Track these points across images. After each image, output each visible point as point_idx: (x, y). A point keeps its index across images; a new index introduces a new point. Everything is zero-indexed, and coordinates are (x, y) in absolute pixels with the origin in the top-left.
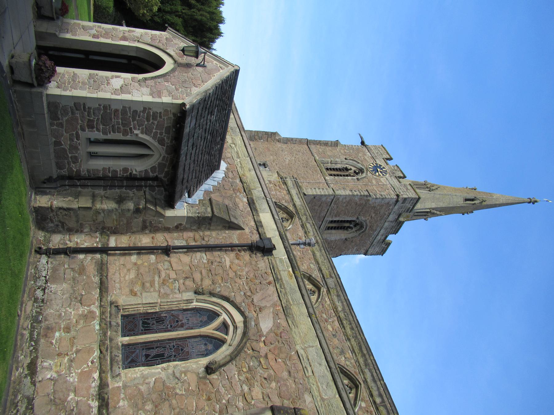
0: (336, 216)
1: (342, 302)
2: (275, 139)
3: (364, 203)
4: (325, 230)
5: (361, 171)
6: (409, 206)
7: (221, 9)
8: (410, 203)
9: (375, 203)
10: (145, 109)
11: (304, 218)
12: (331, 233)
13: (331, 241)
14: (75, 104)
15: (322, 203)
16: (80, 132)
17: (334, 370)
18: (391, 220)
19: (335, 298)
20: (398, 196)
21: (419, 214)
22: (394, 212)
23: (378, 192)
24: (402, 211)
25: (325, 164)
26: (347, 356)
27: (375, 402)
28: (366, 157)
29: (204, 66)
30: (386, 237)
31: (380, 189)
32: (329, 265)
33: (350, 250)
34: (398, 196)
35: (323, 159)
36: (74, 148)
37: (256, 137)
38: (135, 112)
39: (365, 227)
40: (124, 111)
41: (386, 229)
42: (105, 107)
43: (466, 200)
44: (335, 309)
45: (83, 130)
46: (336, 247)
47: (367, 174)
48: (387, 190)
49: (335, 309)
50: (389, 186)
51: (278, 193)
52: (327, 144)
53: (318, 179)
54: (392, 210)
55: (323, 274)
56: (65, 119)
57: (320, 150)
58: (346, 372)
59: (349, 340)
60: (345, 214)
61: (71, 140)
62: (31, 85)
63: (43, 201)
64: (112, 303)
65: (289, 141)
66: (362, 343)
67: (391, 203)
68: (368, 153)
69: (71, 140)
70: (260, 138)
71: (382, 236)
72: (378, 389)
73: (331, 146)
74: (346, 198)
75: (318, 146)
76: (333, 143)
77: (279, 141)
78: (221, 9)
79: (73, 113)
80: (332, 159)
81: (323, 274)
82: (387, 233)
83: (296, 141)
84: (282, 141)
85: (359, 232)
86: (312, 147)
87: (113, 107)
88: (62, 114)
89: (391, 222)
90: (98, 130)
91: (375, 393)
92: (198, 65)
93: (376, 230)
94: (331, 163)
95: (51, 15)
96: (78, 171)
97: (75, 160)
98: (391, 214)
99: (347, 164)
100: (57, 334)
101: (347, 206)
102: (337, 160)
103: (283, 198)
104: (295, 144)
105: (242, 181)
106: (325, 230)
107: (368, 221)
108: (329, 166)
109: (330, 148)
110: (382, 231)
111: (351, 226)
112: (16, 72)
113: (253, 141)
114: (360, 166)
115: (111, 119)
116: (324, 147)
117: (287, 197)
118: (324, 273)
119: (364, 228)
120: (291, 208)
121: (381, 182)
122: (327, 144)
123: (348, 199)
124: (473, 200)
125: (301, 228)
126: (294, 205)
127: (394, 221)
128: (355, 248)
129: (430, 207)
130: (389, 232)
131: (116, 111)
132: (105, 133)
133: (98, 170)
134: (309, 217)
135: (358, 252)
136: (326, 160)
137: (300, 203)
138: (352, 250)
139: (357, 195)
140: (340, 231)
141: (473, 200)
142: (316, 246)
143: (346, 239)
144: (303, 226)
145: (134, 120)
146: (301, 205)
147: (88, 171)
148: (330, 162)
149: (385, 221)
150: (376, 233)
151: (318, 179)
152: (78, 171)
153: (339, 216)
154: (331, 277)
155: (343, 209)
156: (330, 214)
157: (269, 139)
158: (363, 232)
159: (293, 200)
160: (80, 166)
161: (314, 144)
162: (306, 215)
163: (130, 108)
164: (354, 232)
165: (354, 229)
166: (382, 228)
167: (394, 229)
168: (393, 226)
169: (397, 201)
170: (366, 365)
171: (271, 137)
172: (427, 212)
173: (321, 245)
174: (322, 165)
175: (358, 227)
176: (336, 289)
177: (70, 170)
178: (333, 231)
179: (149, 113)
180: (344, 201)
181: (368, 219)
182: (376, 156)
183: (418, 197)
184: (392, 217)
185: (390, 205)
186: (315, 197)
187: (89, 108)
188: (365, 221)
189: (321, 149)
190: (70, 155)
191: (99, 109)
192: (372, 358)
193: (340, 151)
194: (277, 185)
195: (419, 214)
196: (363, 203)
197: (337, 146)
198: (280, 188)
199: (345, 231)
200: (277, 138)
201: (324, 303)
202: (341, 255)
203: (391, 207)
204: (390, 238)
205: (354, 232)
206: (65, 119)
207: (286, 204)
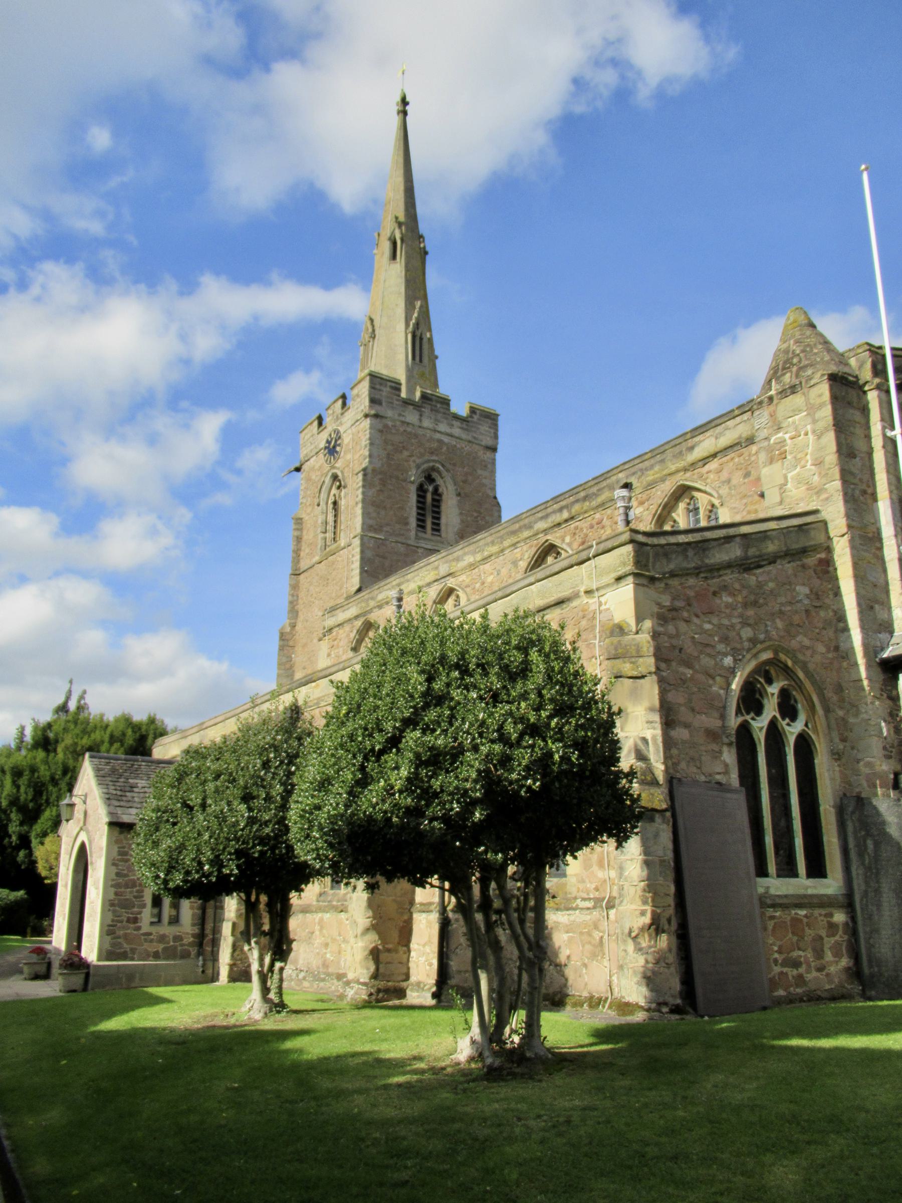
0: (407, 524)
1: (465, 554)
2: (290, 633)
3: (380, 476)
4: (440, 536)
5: (335, 477)
6: (388, 389)
7: (111, 719)
8: (380, 390)
9: (379, 456)
10: (114, 864)
11: (372, 603)
12: (447, 525)
13: (462, 521)
14: (108, 935)
15: (377, 555)
16: (142, 932)
17: (532, 579)
18: (417, 417)
19: (461, 564)
20: (366, 416)
21: (417, 352)
22: (400, 415)
23: (361, 452)
24: (398, 400)
25: (328, 543)
26: (518, 556)
27: (566, 521)
28: (317, 467)
29: (86, 796)
30: (456, 417)
31: (358, 447)
32: (424, 569)
33: (484, 481)
34: (366, 416)
35: (319, 547)
36: (162, 938)
37: (288, 666)
38: (118, 874)
39: (431, 464)
40: (117, 886)
41: (437, 421)
42: (112, 905)
43: (394, 256)
44: (472, 566)
45: (139, 928)
46: (475, 511)
47: (338, 469)
48: (360, 435)
49: (472, 566)
50: (354, 429)
51: (341, 644)
52: (297, 537)
53: (343, 561)
54: (393, 420)
55: (435, 581)
56: (125, 945)
57: (307, 551)
58: (536, 561)
59: (502, 551)
60: (402, 508)
61: (151, 941)
62: (87, 975)
63: (224, 972)
64: (318, 901)
65: (293, 608)
66: (507, 530)
67: (380, 426)
68: (312, 460)
69: (151, 941)
70: (290, 659)
71: (453, 425)
72: (554, 512)
73: (301, 530)
74: (369, 514)
75: (302, 554)
76: (297, 527)
77: (293, 626)
78: (111, 719)
79: (119, 937)
80: (319, 530)
81: (435, 581)
82: (447, 419)
83: (293, 595)
84: (293, 621)
85: (445, 473)
86: (303, 565)
87: (112, 896)
88: (120, 948)
89: (421, 415)
90: (140, 913)
91: (558, 518)
92: (85, 802)
93: (440, 441)
94: (325, 532)
95: (45, 965)
96: (193, 936)
97: (177, 938)
98: (403, 419)
99: (327, 503)
100: (328, 956)
101: (385, 508)
102: (320, 521)
103: (348, 635)
104: (298, 596)
105: (548, 611)
106: (440, 536)
107: (418, 461)
108: (329, 535)
109: (305, 532)
110: (443, 427)
111: (431, 488)
112: (74, 988)
113: (294, 671)
114: (328, 480)
115: (127, 900)
116: (303, 544)
117: (347, 628)
118: (433, 579)
119: (433, 466)
120: (358, 623)
121: (349, 443)
122: (297, 537)
123: (371, 509)
124: (394, 244)
125: (383, 610)
126: (357, 617)
127: (420, 411)
128: (480, 472)
129: (403, 334)
130: (444, 413)
131: (116, 894)
132: (144, 906)
133: (193, 915)
134: (370, 596)
135: (489, 466)
136: (320, 543)
137: (354, 608)
138: (485, 478)
139: (363, 493)
140: (444, 507)
141: (394, 244)
142: (402, 587)
143: (459, 495)
144: (380, 607)
145: (126, 875)
146: (357, 605)
147: (193, 925)
148: (323, 535)
149: (420, 427)
150: (446, 439)
151: (343, 561)
152: (193, 936)
153: (407, 518)
154: (437, 568)
155: (392, 513)
156: (403, 535)
157: (291, 643)
158: (443, 466)
159: (350, 620)
160: (188, 934)
161: (298, 562)
162: (367, 600)
163: (113, 880)
164: (445, 482)
165: (439, 481)
166: (435, 431)
167: (439, 405)
168: (432, 410)
169: (376, 416)
170: (529, 527)
171: (288, 640)
172: (414, 337)
173: (402, 580)
174: (328, 549)
175: (435, 475)
176: (451, 561)
177: (190, 944)
178: (443, 521)
179: (118, 860)
180: (374, 515)
181: (414, 461)
182: (316, 447)
183: (368, 378)
184: (411, 416)
185: (386, 426)
186: (363, 571)
187: (113, 921)
188: (418, 467)
189: (305, 551)
190: (172, 943)
191: (114, 911)
192: (524, 516)
193: (309, 514)
194: (332, 643)
195: (417, 352)
196: (381, 479)
197: (301, 519)
198: (335, 639)
199: (444, 497)
200: (288, 629)
201: (464, 584)
202: (495, 498)
203: (390, 424)
204: (460, 407)
205: (445, 482)
206: (125, 945)
207: (355, 631)
